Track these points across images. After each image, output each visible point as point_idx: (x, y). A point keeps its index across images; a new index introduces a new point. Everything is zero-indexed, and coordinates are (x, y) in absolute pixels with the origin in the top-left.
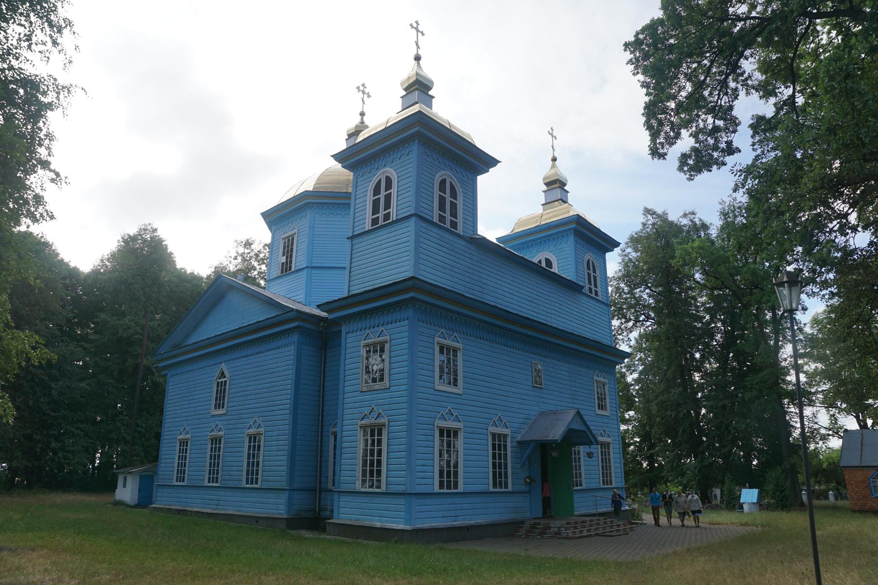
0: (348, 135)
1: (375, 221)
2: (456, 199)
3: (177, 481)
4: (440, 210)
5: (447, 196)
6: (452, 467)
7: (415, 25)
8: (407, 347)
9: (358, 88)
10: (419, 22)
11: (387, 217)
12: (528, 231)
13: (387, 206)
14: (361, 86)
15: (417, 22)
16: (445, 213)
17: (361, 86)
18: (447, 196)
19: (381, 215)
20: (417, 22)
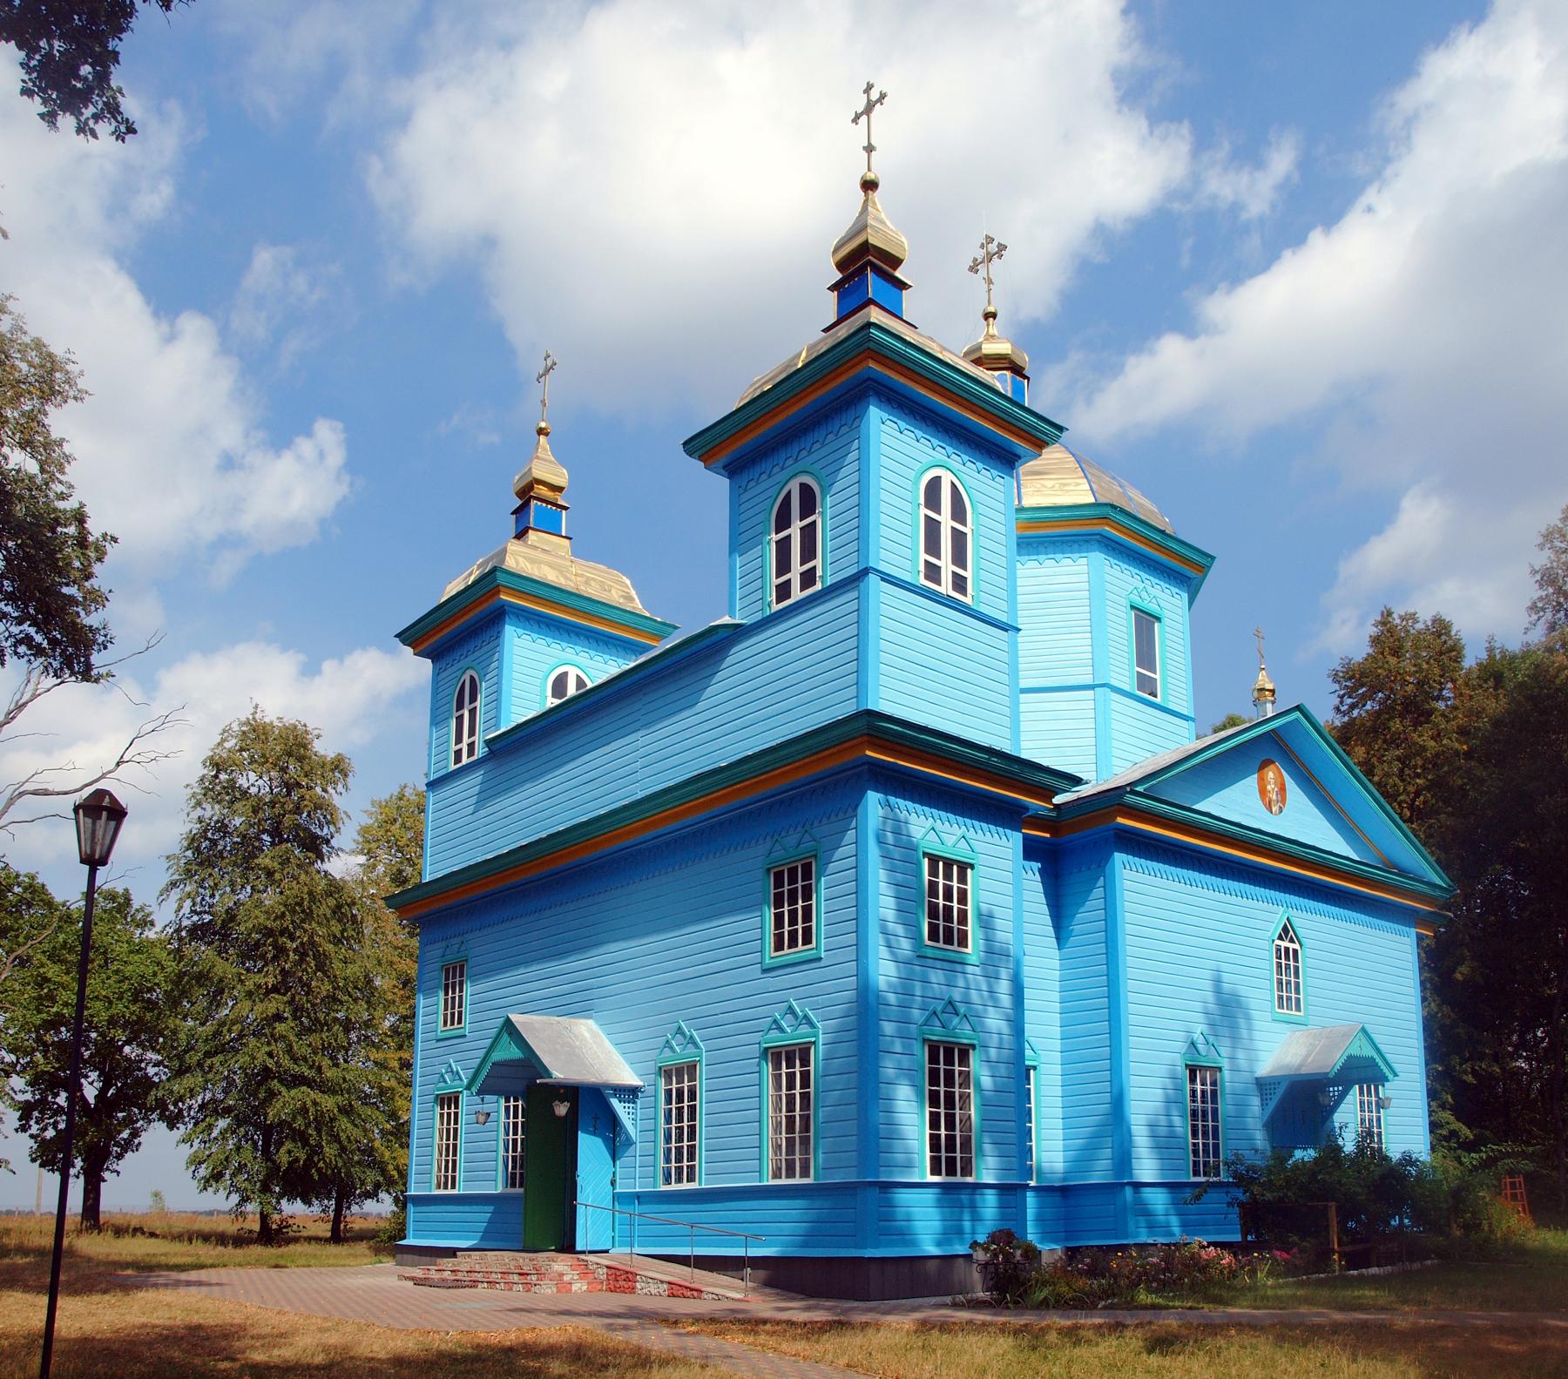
0: (841, 266)
1: (783, 591)
2: (963, 522)
3: (439, 1187)
4: (928, 551)
5: (945, 519)
6: (957, 1085)
7: (874, 95)
8: (856, 1038)
9: (990, 240)
10: (885, 101)
11: (808, 578)
12: (1269, 869)
13: (808, 553)
14: (995, 243)
15: (883, 96)
16: (939, 558)
17: (995, 243)
18: (945, 519)
19: (795, 576)
20: (883, 96)
